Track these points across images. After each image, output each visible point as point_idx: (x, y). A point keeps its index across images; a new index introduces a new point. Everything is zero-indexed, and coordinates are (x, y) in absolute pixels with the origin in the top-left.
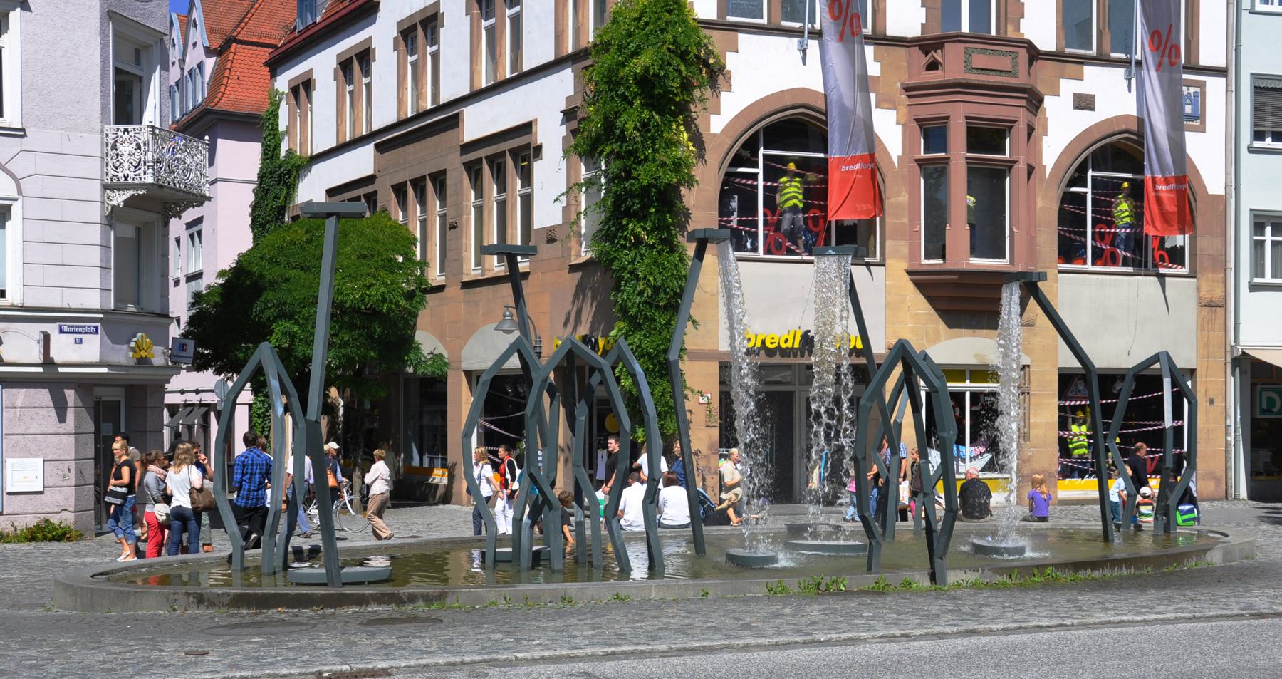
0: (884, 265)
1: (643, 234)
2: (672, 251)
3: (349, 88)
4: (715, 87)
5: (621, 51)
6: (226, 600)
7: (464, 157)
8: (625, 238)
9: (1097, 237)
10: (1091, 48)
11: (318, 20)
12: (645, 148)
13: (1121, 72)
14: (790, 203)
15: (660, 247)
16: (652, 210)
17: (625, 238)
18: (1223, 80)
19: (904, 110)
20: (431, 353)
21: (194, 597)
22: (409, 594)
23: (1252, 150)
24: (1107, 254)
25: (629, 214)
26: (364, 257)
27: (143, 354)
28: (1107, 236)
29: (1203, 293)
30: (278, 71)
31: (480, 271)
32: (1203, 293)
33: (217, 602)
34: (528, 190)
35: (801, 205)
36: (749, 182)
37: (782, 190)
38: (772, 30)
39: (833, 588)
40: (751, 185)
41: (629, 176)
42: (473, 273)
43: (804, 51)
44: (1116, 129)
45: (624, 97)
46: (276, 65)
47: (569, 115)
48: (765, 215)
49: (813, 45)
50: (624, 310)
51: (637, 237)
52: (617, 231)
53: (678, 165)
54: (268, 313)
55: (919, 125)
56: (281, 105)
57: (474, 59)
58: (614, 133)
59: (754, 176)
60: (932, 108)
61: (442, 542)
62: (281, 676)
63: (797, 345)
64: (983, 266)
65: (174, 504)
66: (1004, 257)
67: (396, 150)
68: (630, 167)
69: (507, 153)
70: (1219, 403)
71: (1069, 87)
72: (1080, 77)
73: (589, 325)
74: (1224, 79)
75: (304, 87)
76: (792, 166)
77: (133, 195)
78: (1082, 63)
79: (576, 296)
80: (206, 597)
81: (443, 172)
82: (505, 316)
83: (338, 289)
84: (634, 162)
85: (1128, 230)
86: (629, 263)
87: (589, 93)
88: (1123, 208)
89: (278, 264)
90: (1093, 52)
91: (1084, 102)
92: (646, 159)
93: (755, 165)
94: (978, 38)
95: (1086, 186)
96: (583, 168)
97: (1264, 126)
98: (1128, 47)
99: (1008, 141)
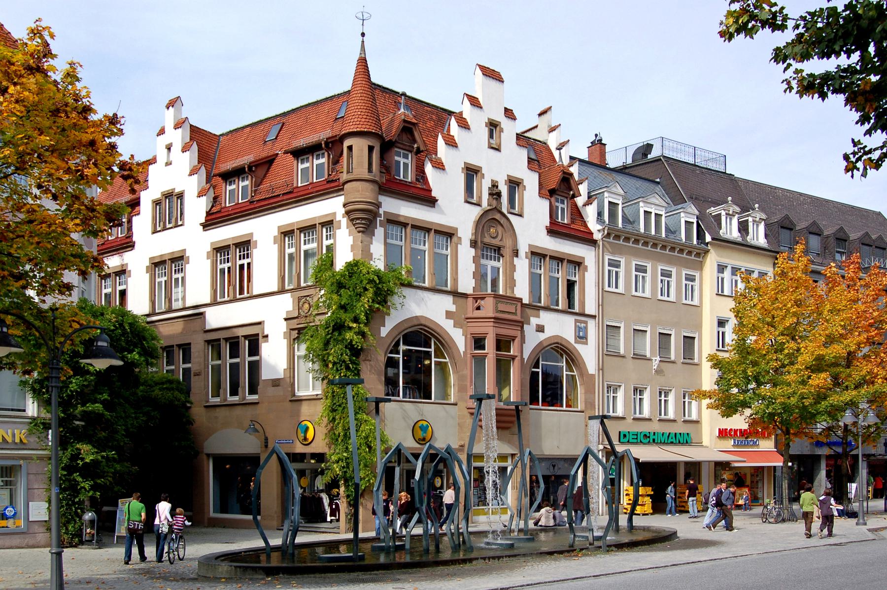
72: (538, 316)
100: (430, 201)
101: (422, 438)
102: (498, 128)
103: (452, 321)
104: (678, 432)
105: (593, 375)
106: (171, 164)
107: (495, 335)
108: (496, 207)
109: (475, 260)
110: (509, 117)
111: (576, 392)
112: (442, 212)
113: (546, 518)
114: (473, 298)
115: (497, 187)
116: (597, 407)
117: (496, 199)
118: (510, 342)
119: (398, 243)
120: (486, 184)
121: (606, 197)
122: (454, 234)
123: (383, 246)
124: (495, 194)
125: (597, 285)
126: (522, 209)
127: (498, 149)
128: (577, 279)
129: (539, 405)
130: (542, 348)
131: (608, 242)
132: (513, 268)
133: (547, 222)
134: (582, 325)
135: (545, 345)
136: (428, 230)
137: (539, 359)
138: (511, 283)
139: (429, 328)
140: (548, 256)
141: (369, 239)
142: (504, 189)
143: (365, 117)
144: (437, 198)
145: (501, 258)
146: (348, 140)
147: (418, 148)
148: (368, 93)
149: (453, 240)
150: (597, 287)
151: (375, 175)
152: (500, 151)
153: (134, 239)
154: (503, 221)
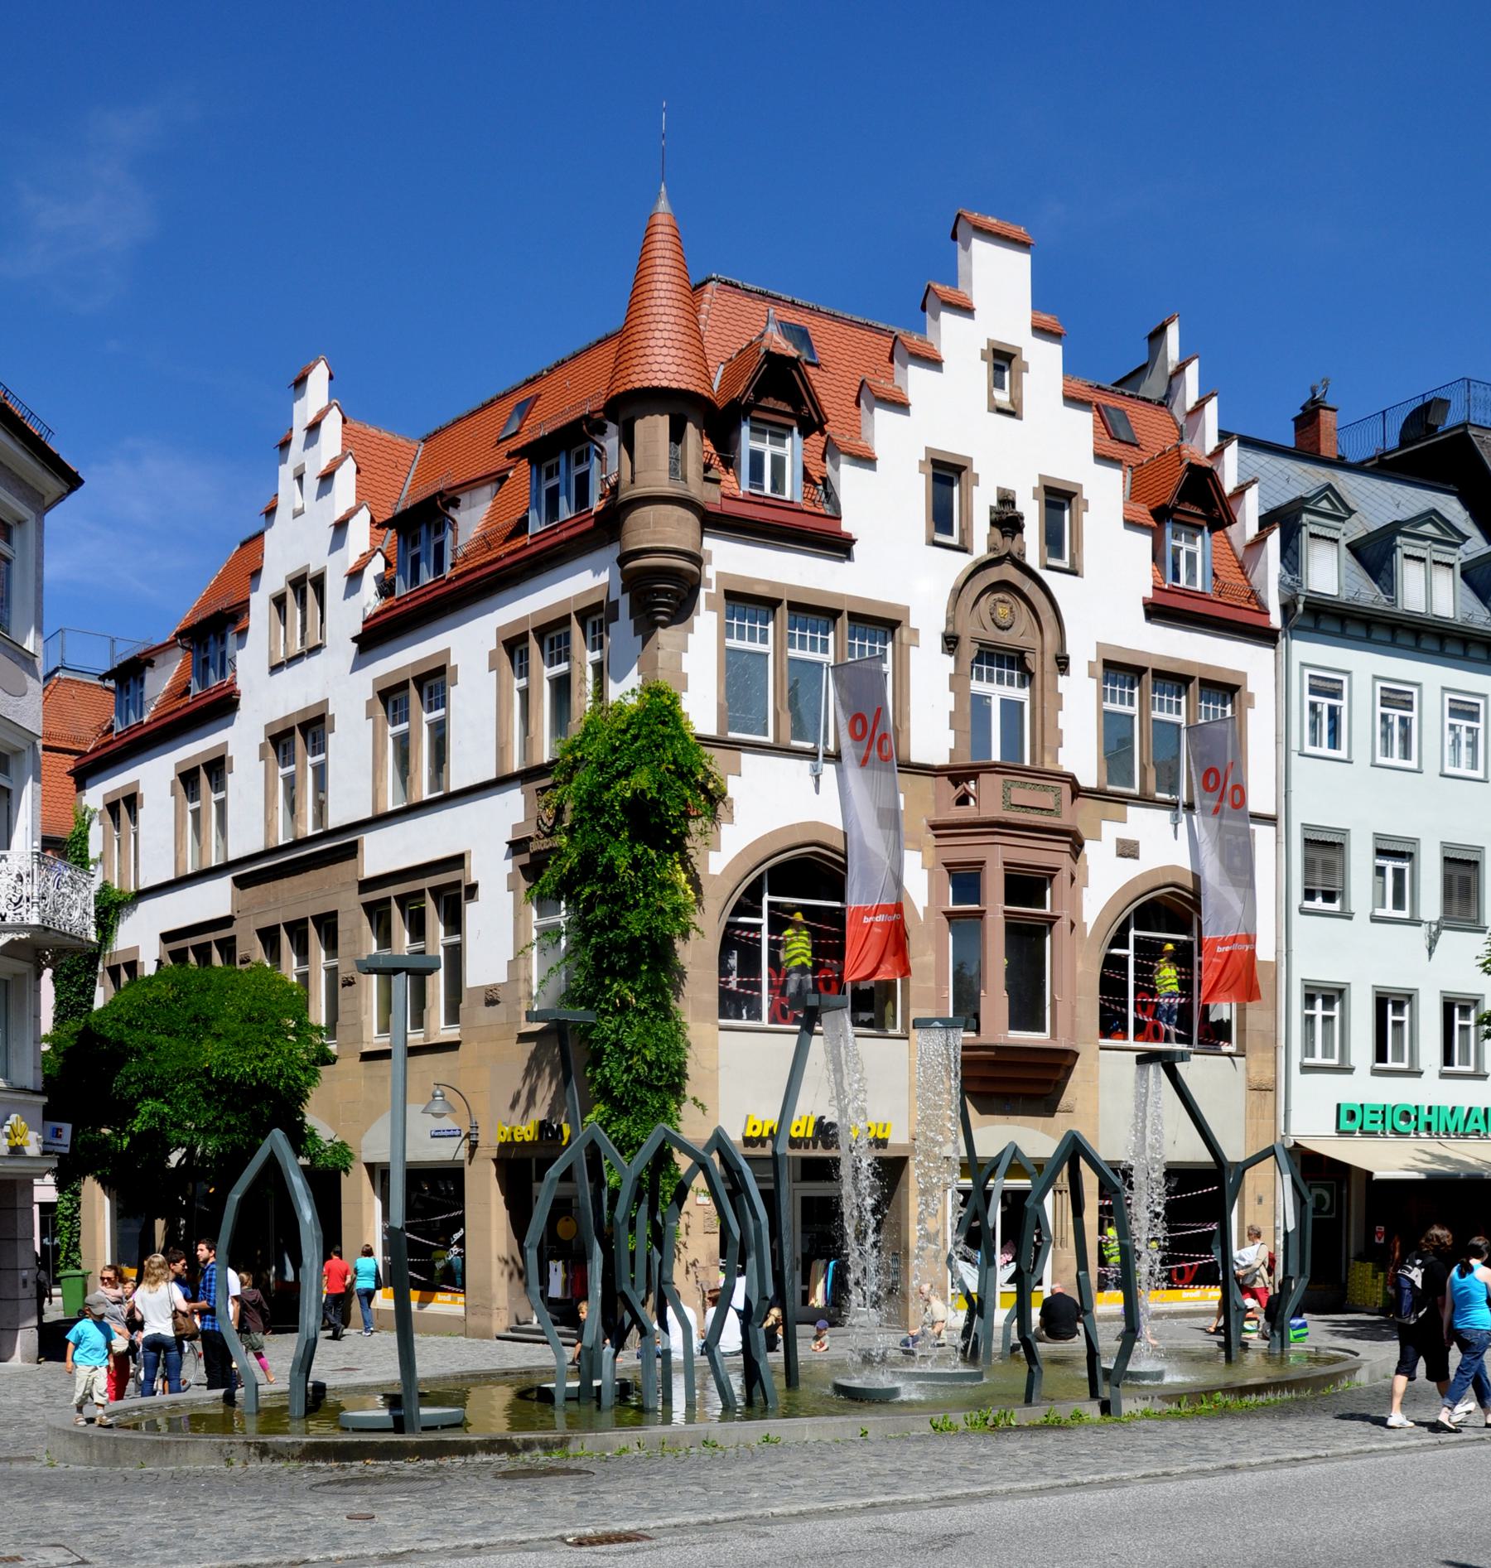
0: (907, 1038)
1: (631, 998)
2: (667, 1019)
3: (191, 806)
4: (714, 818)
5: (601, 770)
6: (297, 1451)
7: (363, 896)
8: (607, 1001)
9: (1139, 1008)
10: (1132, 785)
11: (146, 719)
12: (635, 890)
13: (1165, 815)
14: (797, 962)
15: (653, 1013)
16: (644, 968)
17: (607, 1001)
18: (1273, 829)
19: (931, 852)
20: (331, 1141)
21: (256, 1448)
22: (525, 1440)
23: (1304, 912)
24: (1149, 1029)
25: (615, 974)
26: (251, 1019)
27: (18, 1141)
28: (1149, 1006)
29: (1252, 1075)
30: (88, 782)
31: (422, 1035)
32: (1252, 1075)
33: (285, 1454)
34: (455, 939)
35: (810, 964)
36: (752, 935)
37: (786, 946)
38: (778, 750)
39: (1002, 1422)
40: (754, 938)
41: (614, 924)
42: (375, 1041)
43: (817, 778)
44: (1162, 882)
45: (606, 826)
46: (83, 776)
47: (517, 847)
48: (770, 976)
49: (829, 771)
50: (605, 1093)
51: (623, 1000)
52: (596, 992)
53: (677, 911)
54: (132, 1090)
55: (949, 871)
56: (92, 825)
57: (379, 774)
58: (595, 871)
59: (758, 928)
60: (965, 851)
61: (461, 1377)
62: (520, 1543)
63: (810, 1134)
64: (1019, 1040)
65: (149, 1331)
66: (1043, 1030)
67: (262, 886)
68: (618, 913)
69: (427, 893)
70: (1267, 1201)
71: (1111, 831)
73: (546, 1109)
74: (1273, 828)
75: (126, 806)
76: (798, 916)
77: (12, 941)
78: (1125, 803)
79: (528, 1071)
80: (270, 1446)
81: (334, 914)
82: (434, 1096)
83: (223, 1061)
84: (622, 909)
85: (1183, 1000)
86: (612, 1032)
87: (545, 820)
88: (1167, 976)
89: (141, 1027)
90: (1136, 790)
91: (1128, 850)
92: (636, 904)
93: (759, 914)
94: (1010, 769)
95: (1127, 947)
96: (534, 913)
97: (1314, 884)
98: (1173, 788)
99: (1048, 892)
100: (839, 546)
104: (1434, 1104)
106: (1350, 918)
109: (957, 682)
115: (1013, 503)
120: (983, 502)
124: (1007, 522)
127: (1013, 413)
138: (1048, 736)
142: (1031, 511)
144: (854, 537)
153: (238, 687)
154: (1028, 586)
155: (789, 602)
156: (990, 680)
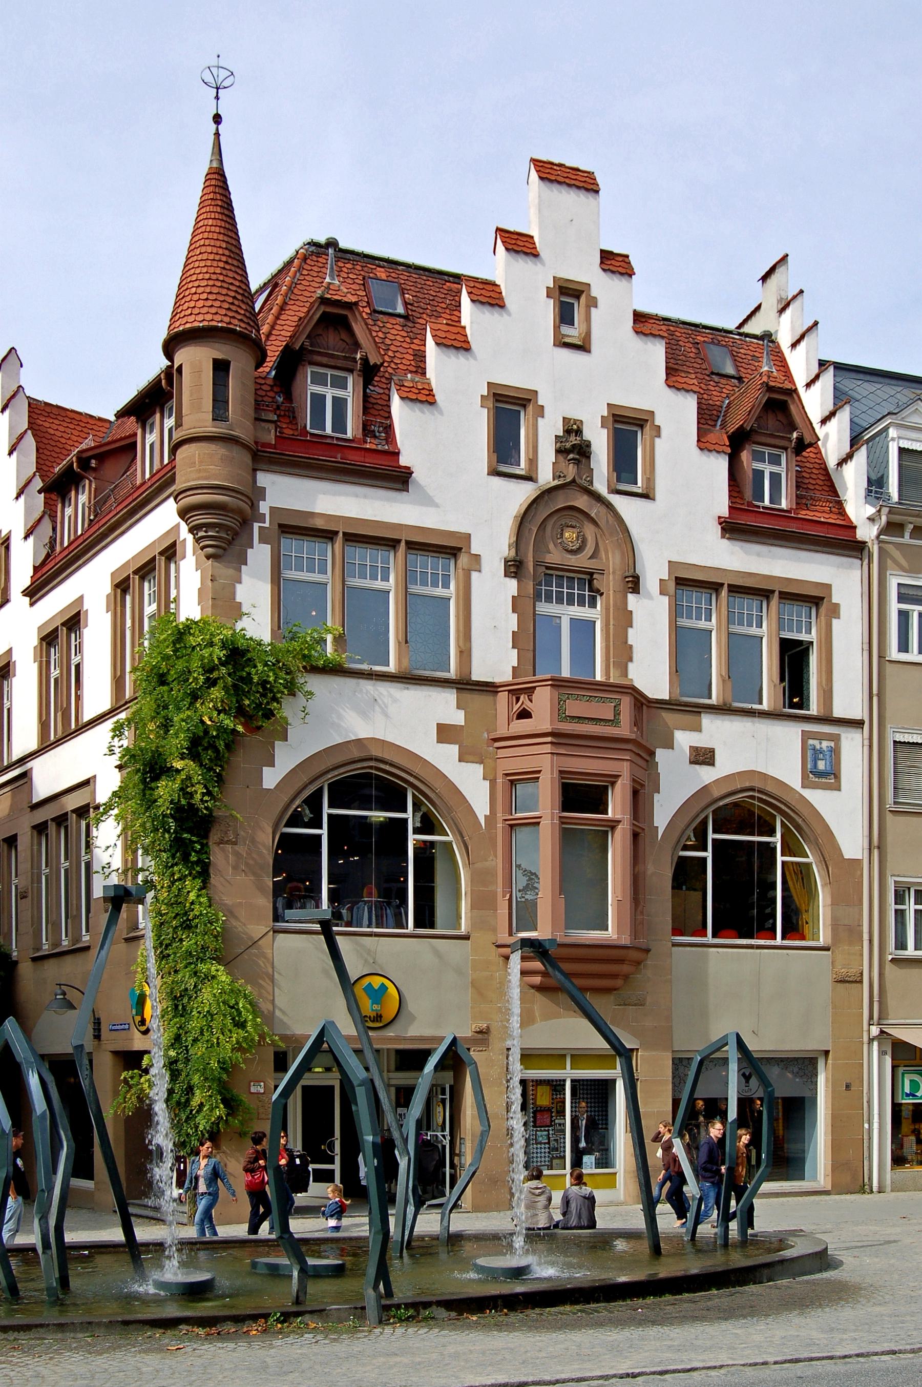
71: (684, 740)
72: (698, 729)
95: (321, 827)
101: (373, 1014)
102: (583, 298)
103: (455, 749)
105: (857, 862)
107: (556, 775)
108: (574, 481)
110: (613, 272)
111: (816, 904)
112: (427, 501)
113: (528, 1207)
114: (509, 691)
115: (579, 432)
116: (866, 936)
117: (577, 462)
118: (606, 788)
119: (316, 577)
121: (893, 439)
122: (460, 549)
123: (268, 587)
125: (866, 647)
126: (650, 480)
127: (583, 347)
128: (813, 636)
129: (706, 936)
130: (709, 800)
131: (898, 546)
132: (625, 619)
133: (722, 505)
134: (825, 744)
135: (716, 793)
136: (716, 587)
137: (704, 823)
139: (391, 765)
140: (726, 587)
141: (231, 572)
143: (204, 296)
145: (598, 597)
146: (182, 350)
147: (365, 360)
148: (218, 244)
149: (459, 562)
150: (866, 654)
151: (231, 425)
152: (589, 351)
154: (595, 510)
155: (728, 584)
156: (560, 601)
